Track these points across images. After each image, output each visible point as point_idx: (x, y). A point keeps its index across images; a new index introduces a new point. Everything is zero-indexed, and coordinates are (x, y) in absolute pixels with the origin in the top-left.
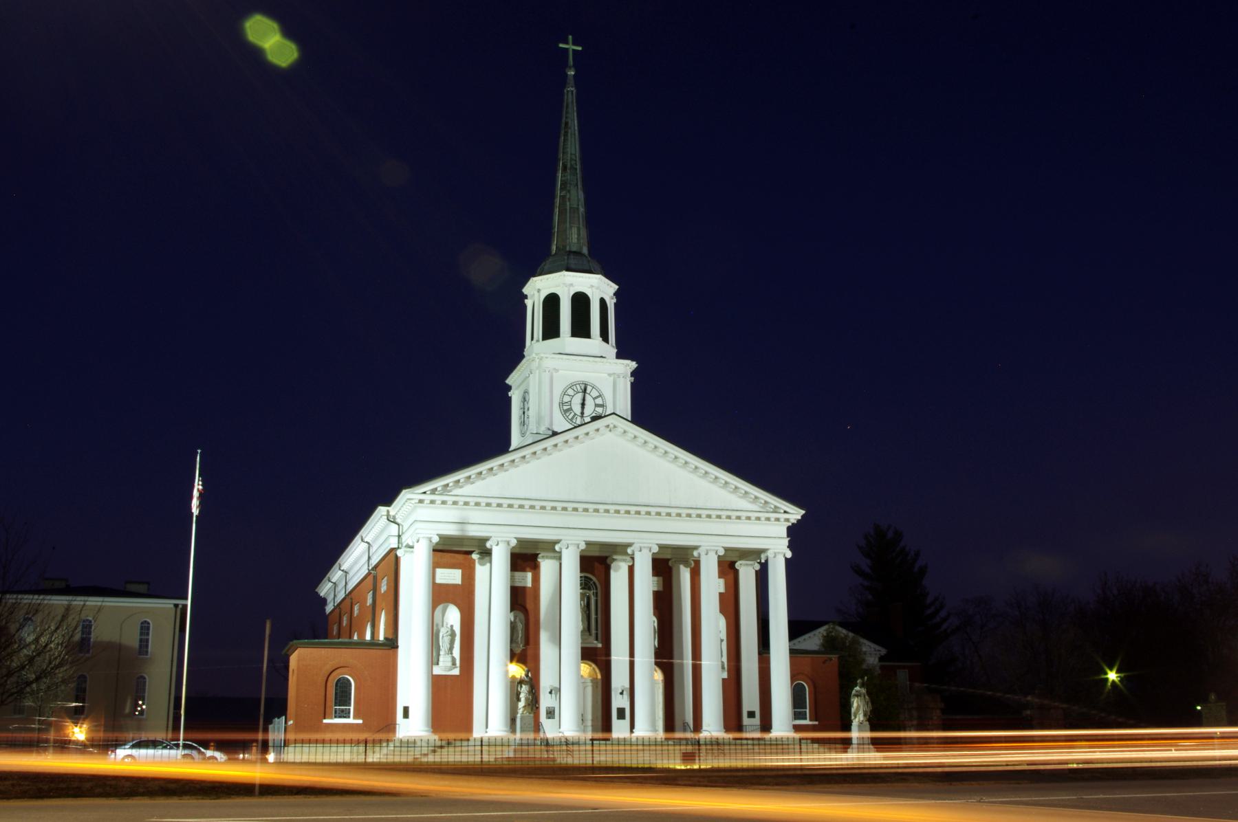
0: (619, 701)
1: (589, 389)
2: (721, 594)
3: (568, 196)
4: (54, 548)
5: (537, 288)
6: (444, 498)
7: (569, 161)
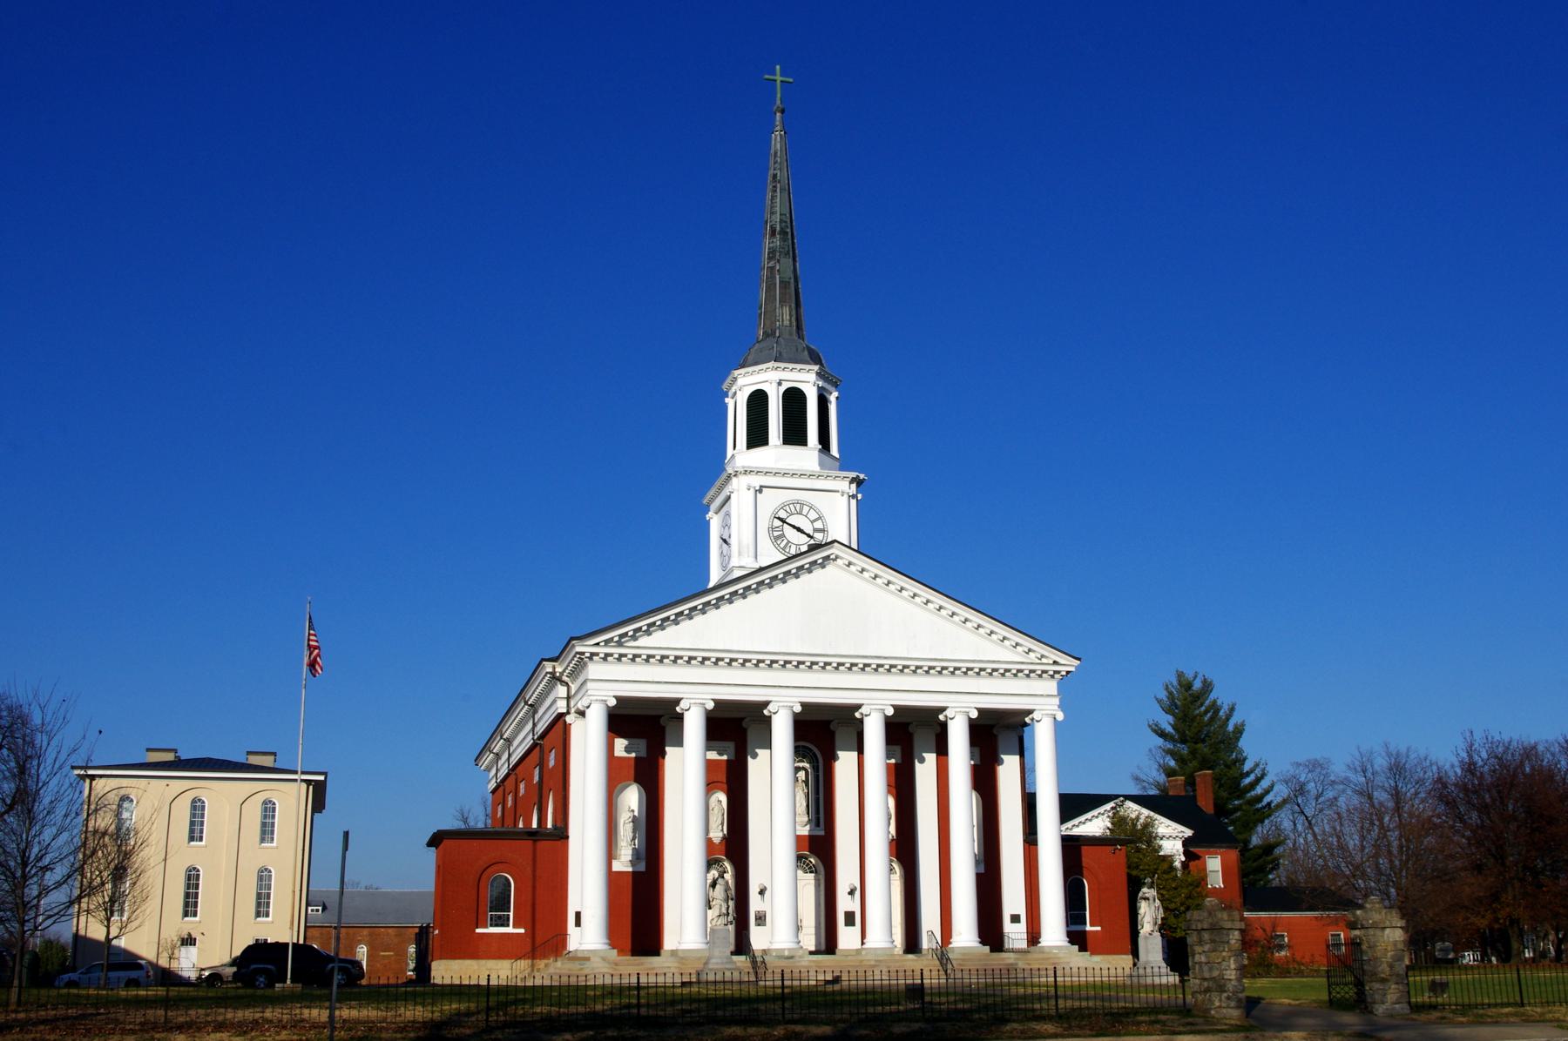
0: (844, 903)
1: (782, 514)
3: (778, 268)
4: (100, 732)
5: (746, 381)
6: (623, 651)
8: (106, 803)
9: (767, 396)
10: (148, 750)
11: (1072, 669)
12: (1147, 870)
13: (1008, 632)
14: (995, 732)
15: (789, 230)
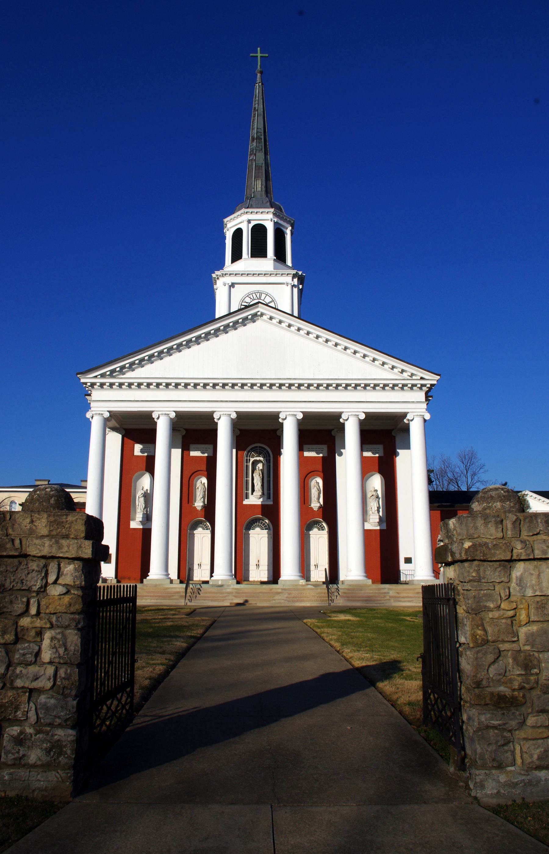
2: (344, 448)
7: (256, 134)
8: (4, 504)
9: (242, 230)
10: (36, 480)
11: (435, 382)
13: (406, 366)
14: (393, 434)
15: (262, 137)
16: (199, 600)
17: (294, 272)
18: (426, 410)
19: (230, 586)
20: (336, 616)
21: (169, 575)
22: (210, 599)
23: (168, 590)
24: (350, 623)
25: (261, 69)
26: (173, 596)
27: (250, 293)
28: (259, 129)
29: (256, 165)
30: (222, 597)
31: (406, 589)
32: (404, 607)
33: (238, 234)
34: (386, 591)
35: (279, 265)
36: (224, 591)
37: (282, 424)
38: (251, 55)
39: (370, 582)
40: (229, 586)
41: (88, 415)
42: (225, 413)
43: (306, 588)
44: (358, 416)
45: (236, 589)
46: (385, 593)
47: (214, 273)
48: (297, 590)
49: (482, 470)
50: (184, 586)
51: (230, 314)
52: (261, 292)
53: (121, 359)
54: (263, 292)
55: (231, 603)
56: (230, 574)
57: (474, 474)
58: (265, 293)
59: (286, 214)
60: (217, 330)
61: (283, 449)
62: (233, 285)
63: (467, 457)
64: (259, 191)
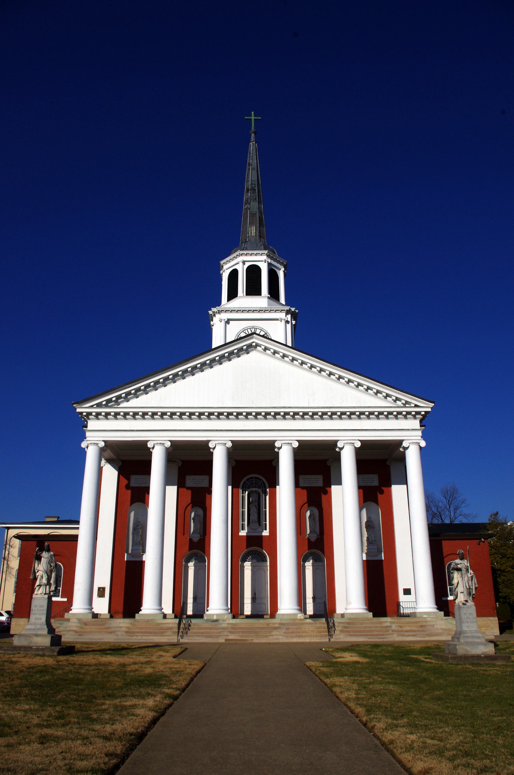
7: (250, 185)
11: (429, 410)
12: (512, 557)
13: (400, 394)
14: (388, 463)
15: (256, 188)
16: (191, 636)
17: (287, 308)
18: (422, 438)
19: (226, 621)
20: (340, 656)
21: (163, 609)
22: (205, 635)
23: (161, 626)
24: (360, 666)
25: (255, 130)
26: (165, 632)
27: (245, 329)
28: (253, 181)
29: (251, 213)
30: (217, 633)
31: (409, 623)
32: (410, 642)
33: (234, 274)
34: (388, 624)
35: (272, 302)
36: (219, 626)
37: (278, 453)
38: (246, 118)
39: (371, 614)
40: (224, 620)
41: (83, 445)
42: (220, 442)
43: (305, 622)
44: (354, 444)
45: (232, 624)
46: (387, 627)
47: (211, 310)
48: (296, 624)
49: (464, 505)
50: (177, 621)
51: (226, 344)
52: (256, 327)
53: (117, 389)
54: (258, 328)
55: (226, 640)
56: (226, 608)
57: (456, 509)
58: (259, 328)
59: (278, 255)
60: (213, 361)
61: (279, 485)
62: (228, 322)
63: (449, 492)
64: (253, 236)
